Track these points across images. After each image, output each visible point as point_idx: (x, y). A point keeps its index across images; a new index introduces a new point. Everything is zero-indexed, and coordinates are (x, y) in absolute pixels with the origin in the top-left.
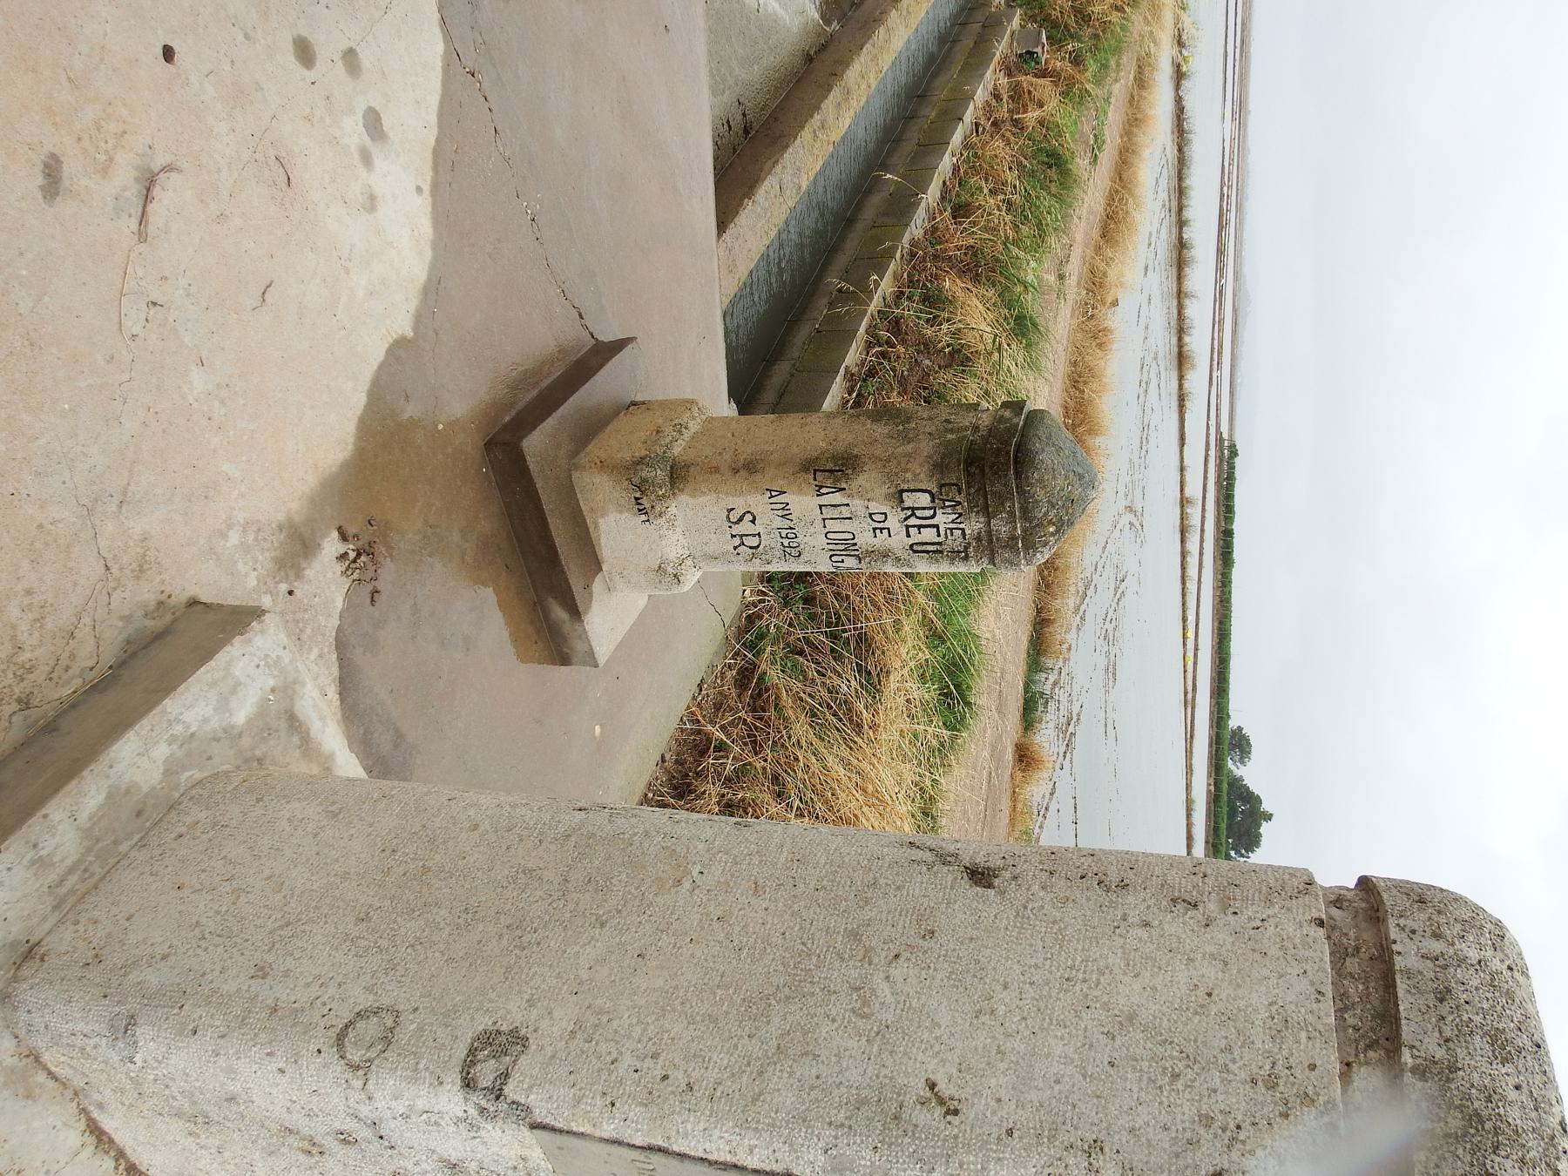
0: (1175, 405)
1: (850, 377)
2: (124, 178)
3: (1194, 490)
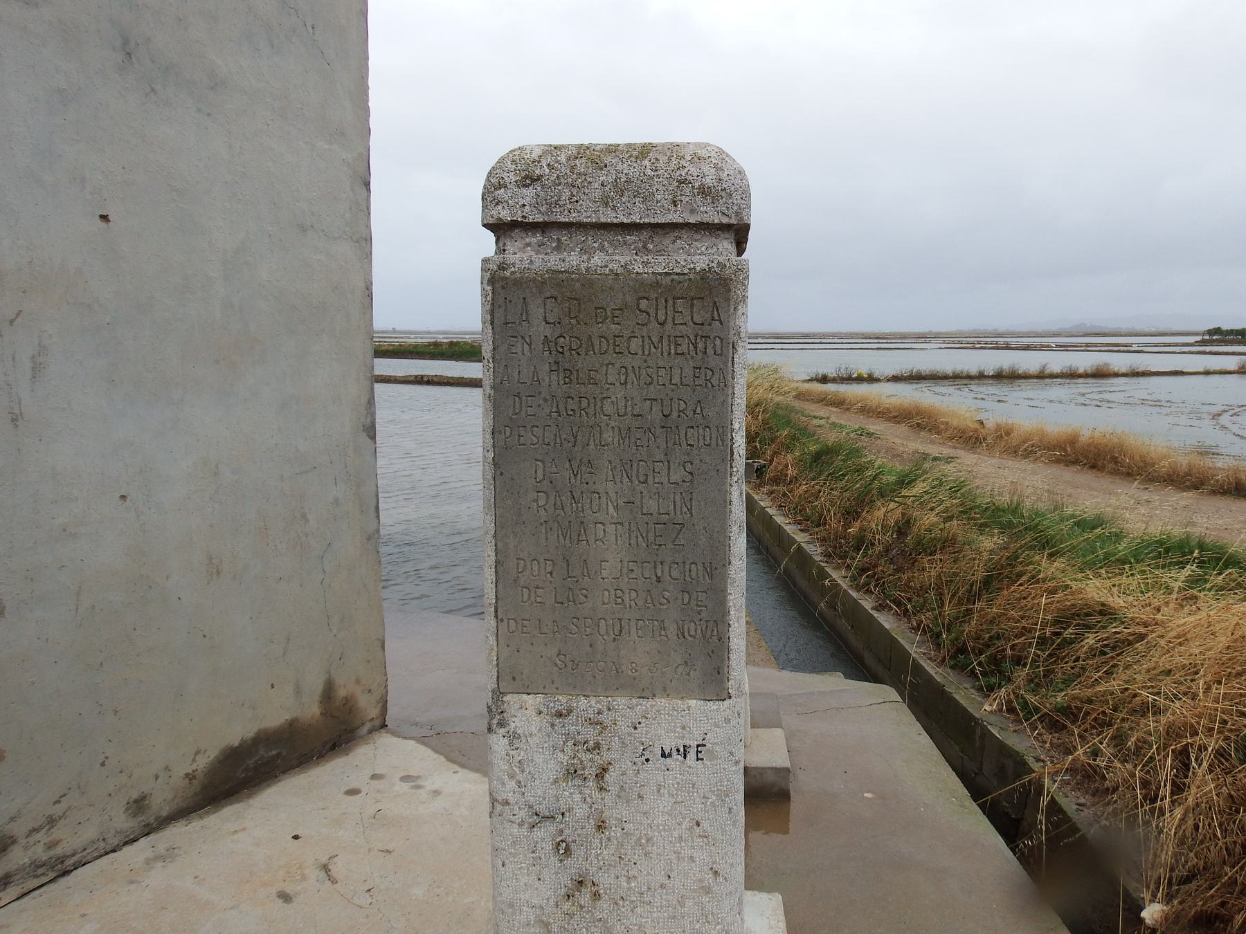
0: (1141, 380)
1: (880, 607)
2: (314, 874)
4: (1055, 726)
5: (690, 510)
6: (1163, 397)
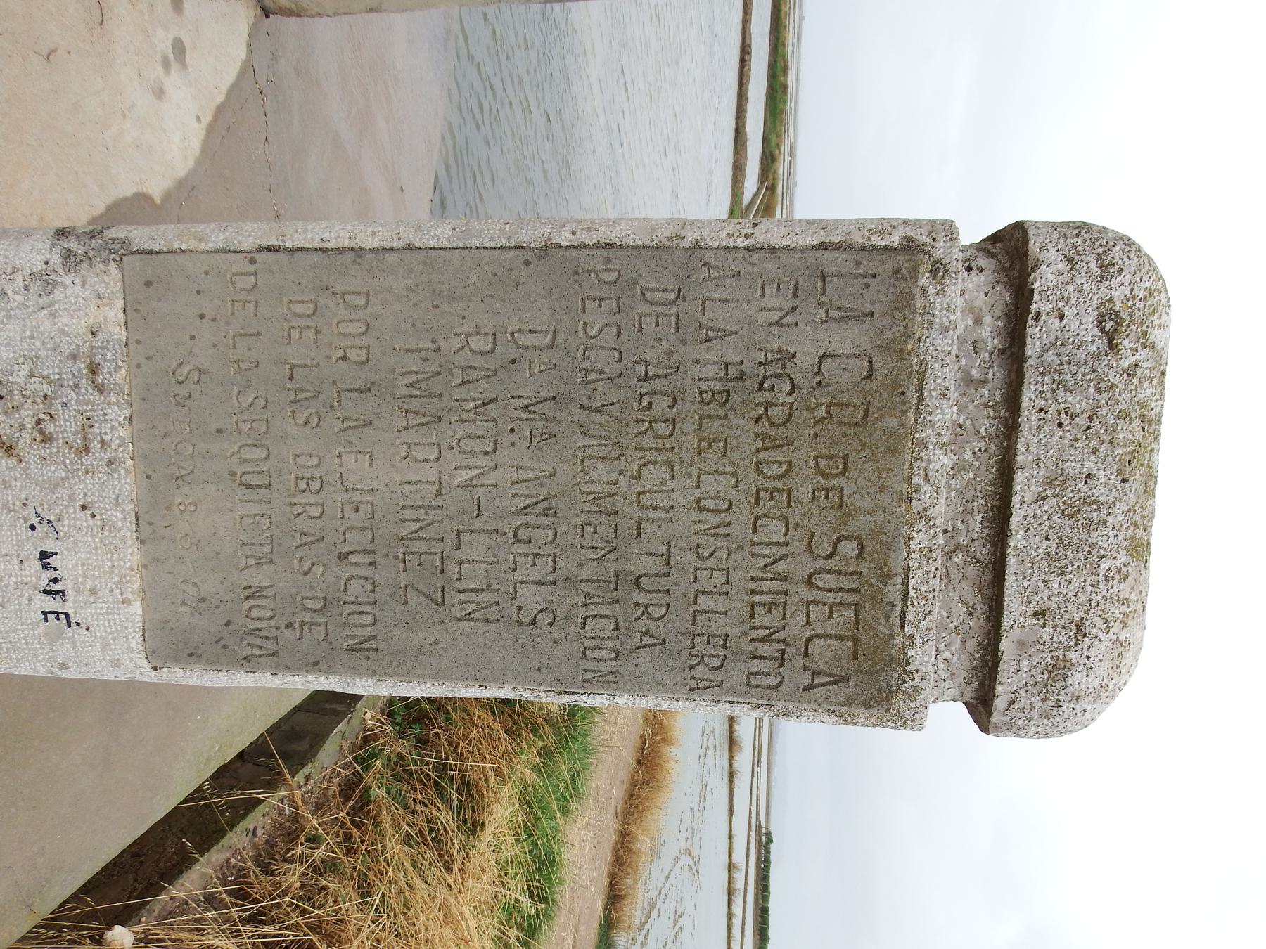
0: (726, 779)
3: (739, 857)
4: (349, 788)
5: (468, 618)
6: (708, 803)
